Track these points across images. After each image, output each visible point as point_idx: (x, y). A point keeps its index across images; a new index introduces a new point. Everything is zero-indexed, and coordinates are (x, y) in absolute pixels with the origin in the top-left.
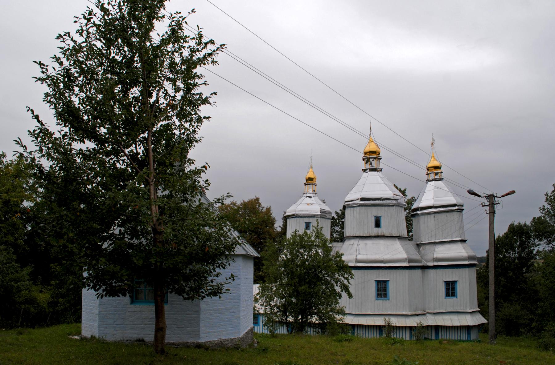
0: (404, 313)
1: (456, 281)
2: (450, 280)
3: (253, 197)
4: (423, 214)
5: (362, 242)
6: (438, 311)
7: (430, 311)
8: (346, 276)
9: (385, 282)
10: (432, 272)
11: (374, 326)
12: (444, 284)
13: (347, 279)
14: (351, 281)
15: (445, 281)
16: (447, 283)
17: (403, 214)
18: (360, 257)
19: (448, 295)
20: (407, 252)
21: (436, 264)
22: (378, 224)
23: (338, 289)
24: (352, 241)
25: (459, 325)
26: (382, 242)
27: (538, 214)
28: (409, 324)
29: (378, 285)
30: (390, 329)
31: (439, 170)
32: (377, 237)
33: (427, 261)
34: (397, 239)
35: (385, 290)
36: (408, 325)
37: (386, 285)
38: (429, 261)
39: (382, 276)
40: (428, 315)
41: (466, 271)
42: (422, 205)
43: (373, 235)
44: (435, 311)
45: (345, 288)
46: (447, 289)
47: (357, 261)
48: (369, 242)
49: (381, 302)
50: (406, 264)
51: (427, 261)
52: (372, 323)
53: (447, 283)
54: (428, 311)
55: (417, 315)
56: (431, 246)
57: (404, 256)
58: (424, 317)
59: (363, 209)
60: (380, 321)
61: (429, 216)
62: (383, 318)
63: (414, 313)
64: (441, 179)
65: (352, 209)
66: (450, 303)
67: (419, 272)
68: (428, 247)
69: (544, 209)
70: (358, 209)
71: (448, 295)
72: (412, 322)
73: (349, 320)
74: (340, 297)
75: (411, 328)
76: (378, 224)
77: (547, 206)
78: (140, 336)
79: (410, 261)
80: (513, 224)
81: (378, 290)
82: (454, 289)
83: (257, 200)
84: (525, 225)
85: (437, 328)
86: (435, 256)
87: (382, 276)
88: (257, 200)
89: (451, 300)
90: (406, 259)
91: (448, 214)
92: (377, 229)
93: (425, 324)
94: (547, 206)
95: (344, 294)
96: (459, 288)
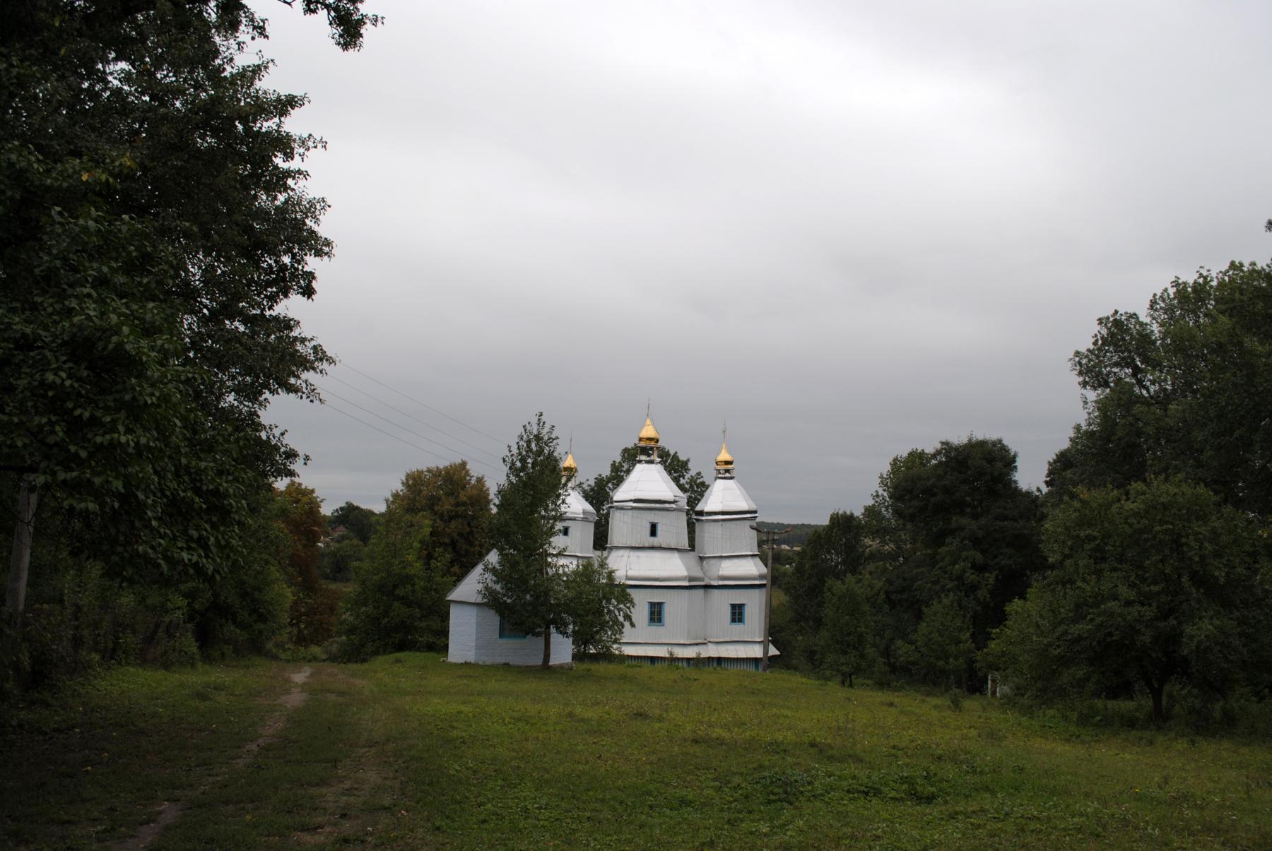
0: (682, 642)
1: (744, 604)
2: (738, 602)
3: (458, 461)
4: (708, 521)
5: (634, 554)
6: (721, 640)
7: (712, 640)
8: (628, 605)
9: (660, 604)
10: (716, 592)
11: (645, 657)
12: (729, 607)
13: (629, 608)
14: (632, 609)
15: (732, 605)
16: (733, 606)
17: (683, 519)
18: (631, 573)
19: (733, 620)
20: (688, 569)
21: (721, 583)
22: (653, 532)
23: (621, 619)
24: (621, 552)
25: (745, 656)
26: (657, 555)
27: (871, 502)
28: (686, 656)
29: (651, 608)
30: (673, 660)
31: (730, 467)
32: (652, 548)
33: (710, 579)
34: (676, 552)
35: (660, 613)
36: (686, 656)
37: (660, 608)
38: (714, 580)
39: (656, 597)
40: (709, 644)
41: (756, 592)
42: (707, 509)
43: (647, 545)
44: (718, 641)
45: (628, 618)
46: (733, 614)
47: (628, 578)
48: (642, 554)
49: (655, 629)
50: (686, 584)
51: (710, 579)
52: (743, 655)
53: (733, 606)
54: (709, 640)
55: (697, 644)
56: (717, 560)
57: (684, 573)
58: (704, 647)
59: (636, 513)
60: (661, 652)
61: (716, 523)
62: (665, 648)
63: (693, 642)
64: (731, 478)
65: (622, 511)
66: (737, 631)
67: (701, 592)
68: (712, 561)
69: (878, 496)
70: (630, 512)
71: (733, 620)
72: (690, 653)
73: (629, 651)
74: (623, 626)
75: (688, 660)
76: (653, 532)
77: (881, 492)
78: (507, 661)
79: (691, 579)
80: (838, 514)
81: (652, 613)
82: (741, 614)
83: (464, 464)
84: (852, 515)
85: (720, 660)
86: (720, 573)
87: (656, 597)
88: (464, 464)
89: (737, 626)
90: (686, 577)
91: (738, 522)
92: (653, 538)
93: (704, 655)
94: (881, 492)
95: (627, 624)
96: (748, 613)
